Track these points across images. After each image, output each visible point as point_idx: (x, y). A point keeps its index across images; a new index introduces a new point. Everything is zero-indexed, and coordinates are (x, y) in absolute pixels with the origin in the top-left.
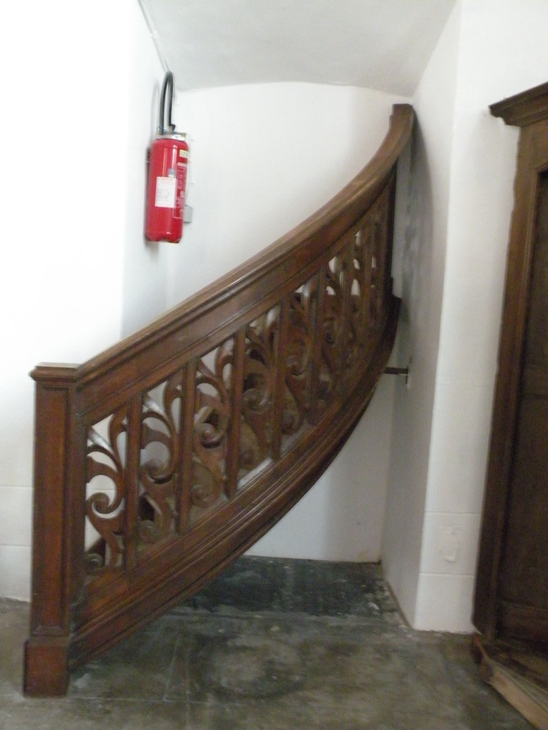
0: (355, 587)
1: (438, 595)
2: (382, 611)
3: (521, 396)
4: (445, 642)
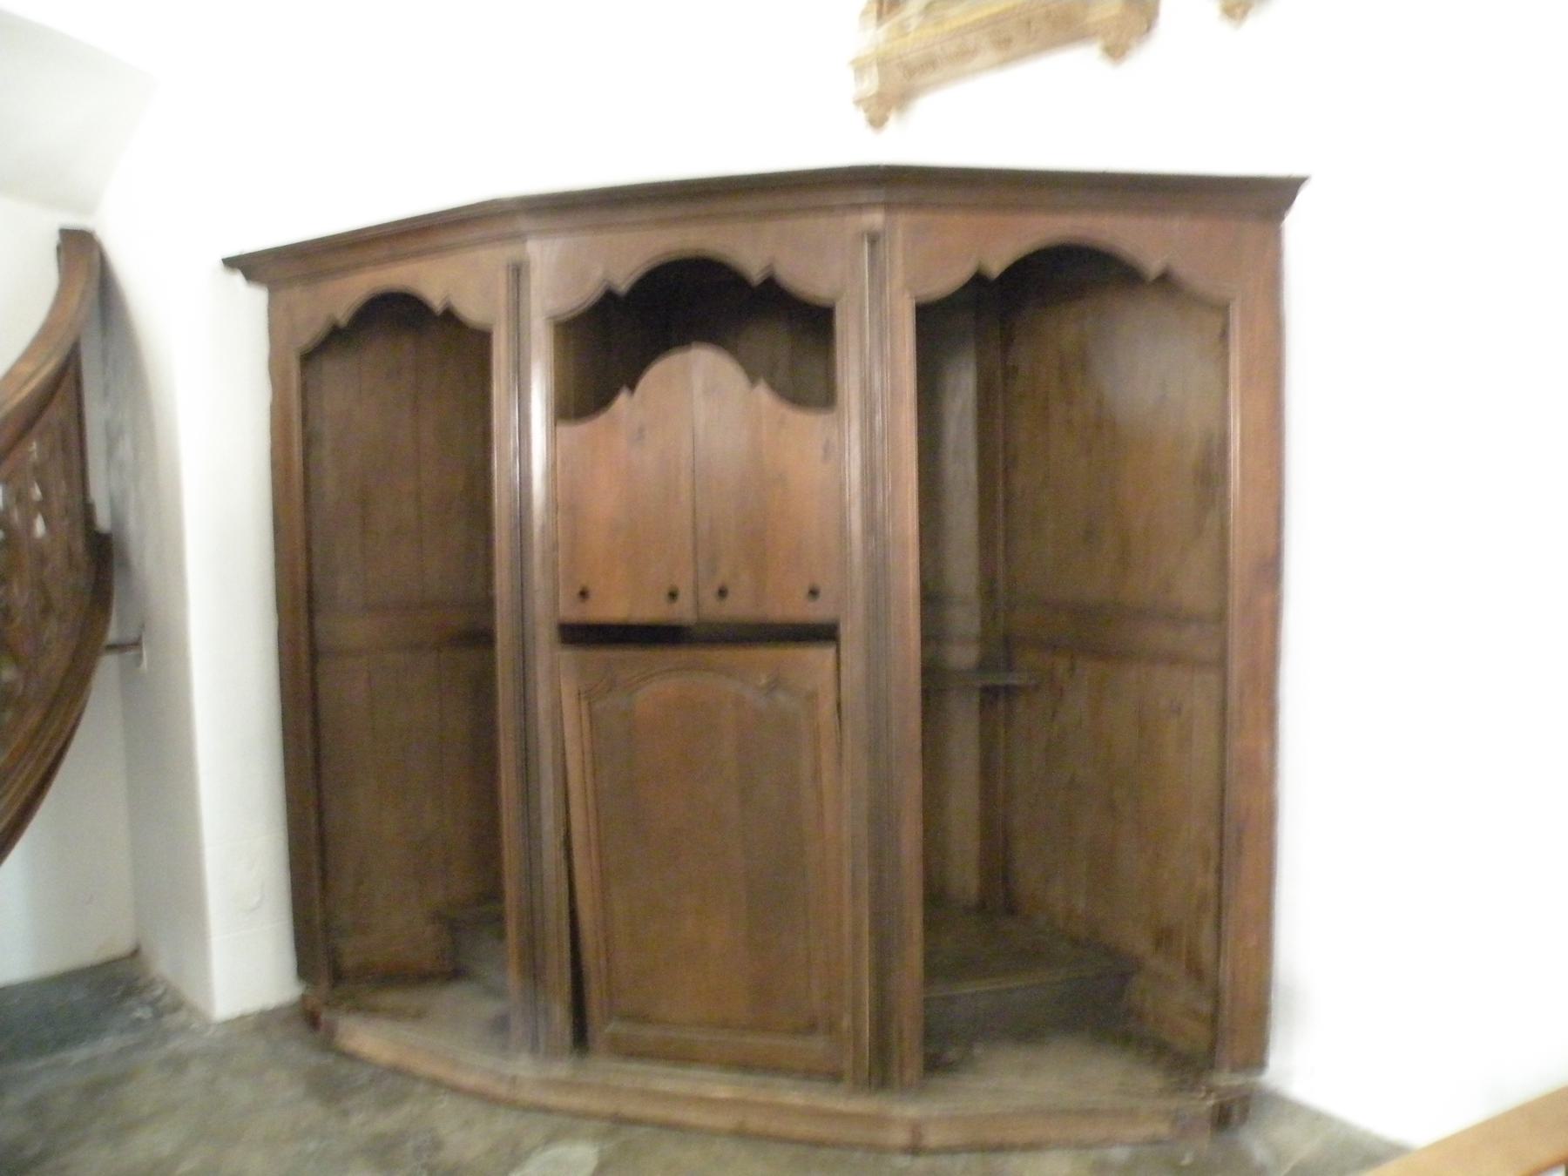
0: (111, 993)
1: (240, 958)
2: (158, 1015)
3: (314, 655)
4: (263, 1022)
